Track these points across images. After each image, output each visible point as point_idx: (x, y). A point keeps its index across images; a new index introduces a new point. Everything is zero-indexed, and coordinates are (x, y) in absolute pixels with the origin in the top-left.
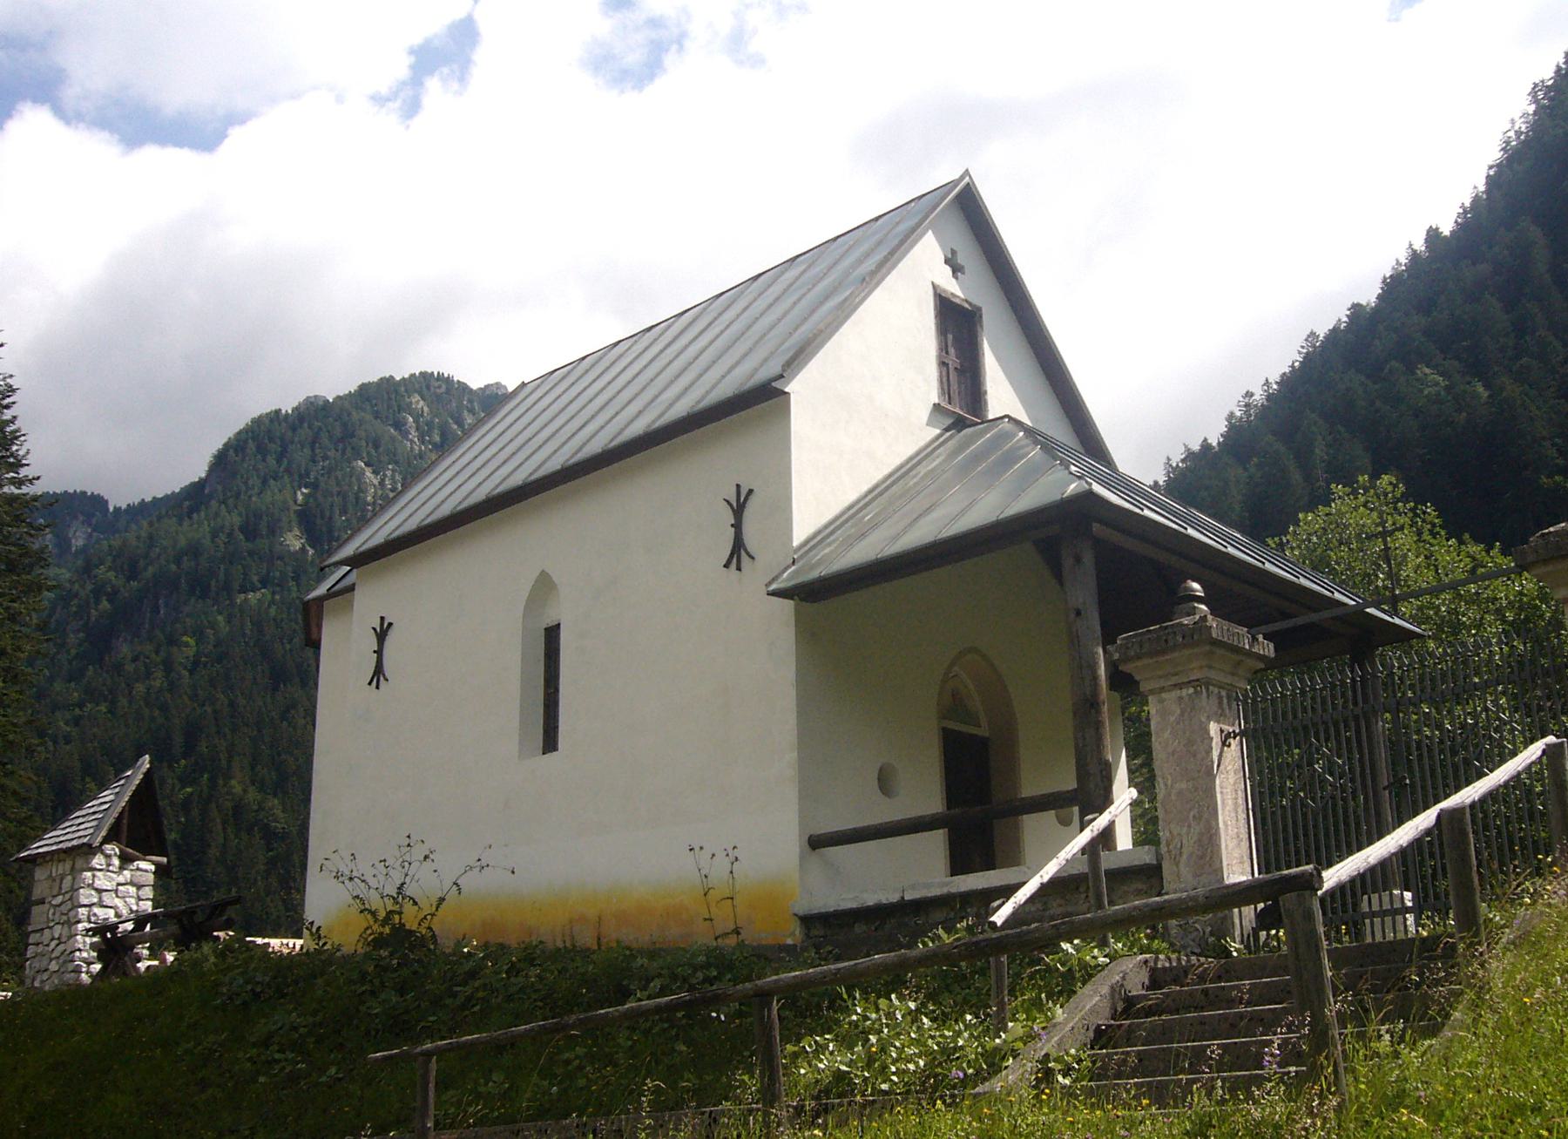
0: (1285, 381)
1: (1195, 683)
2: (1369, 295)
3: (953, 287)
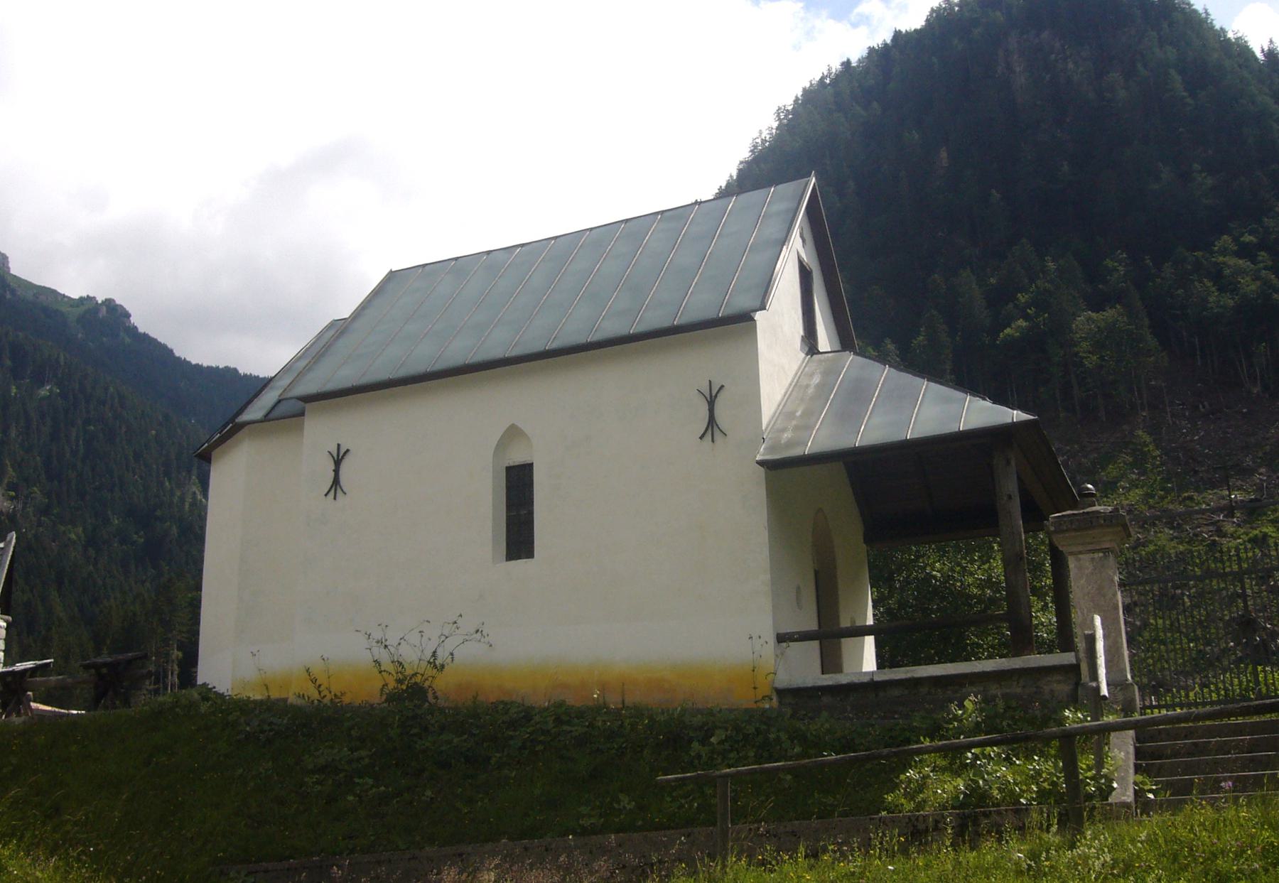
1: (1106, 551)
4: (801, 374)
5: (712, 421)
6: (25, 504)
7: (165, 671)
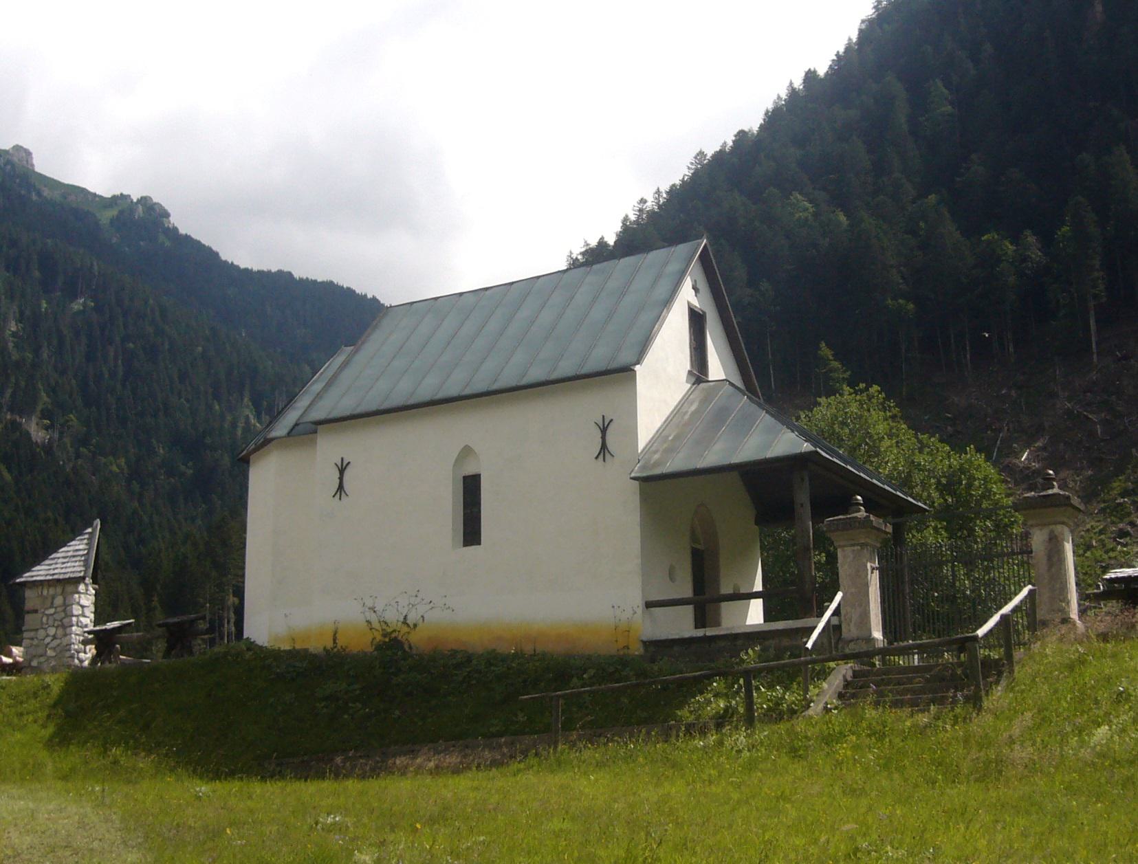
0: (673, 191)
2: (753, 123)
3: (695, 303)
4: (685, 400)
5: (604, 447)
6: (61, 433)
7: (221, 619)
